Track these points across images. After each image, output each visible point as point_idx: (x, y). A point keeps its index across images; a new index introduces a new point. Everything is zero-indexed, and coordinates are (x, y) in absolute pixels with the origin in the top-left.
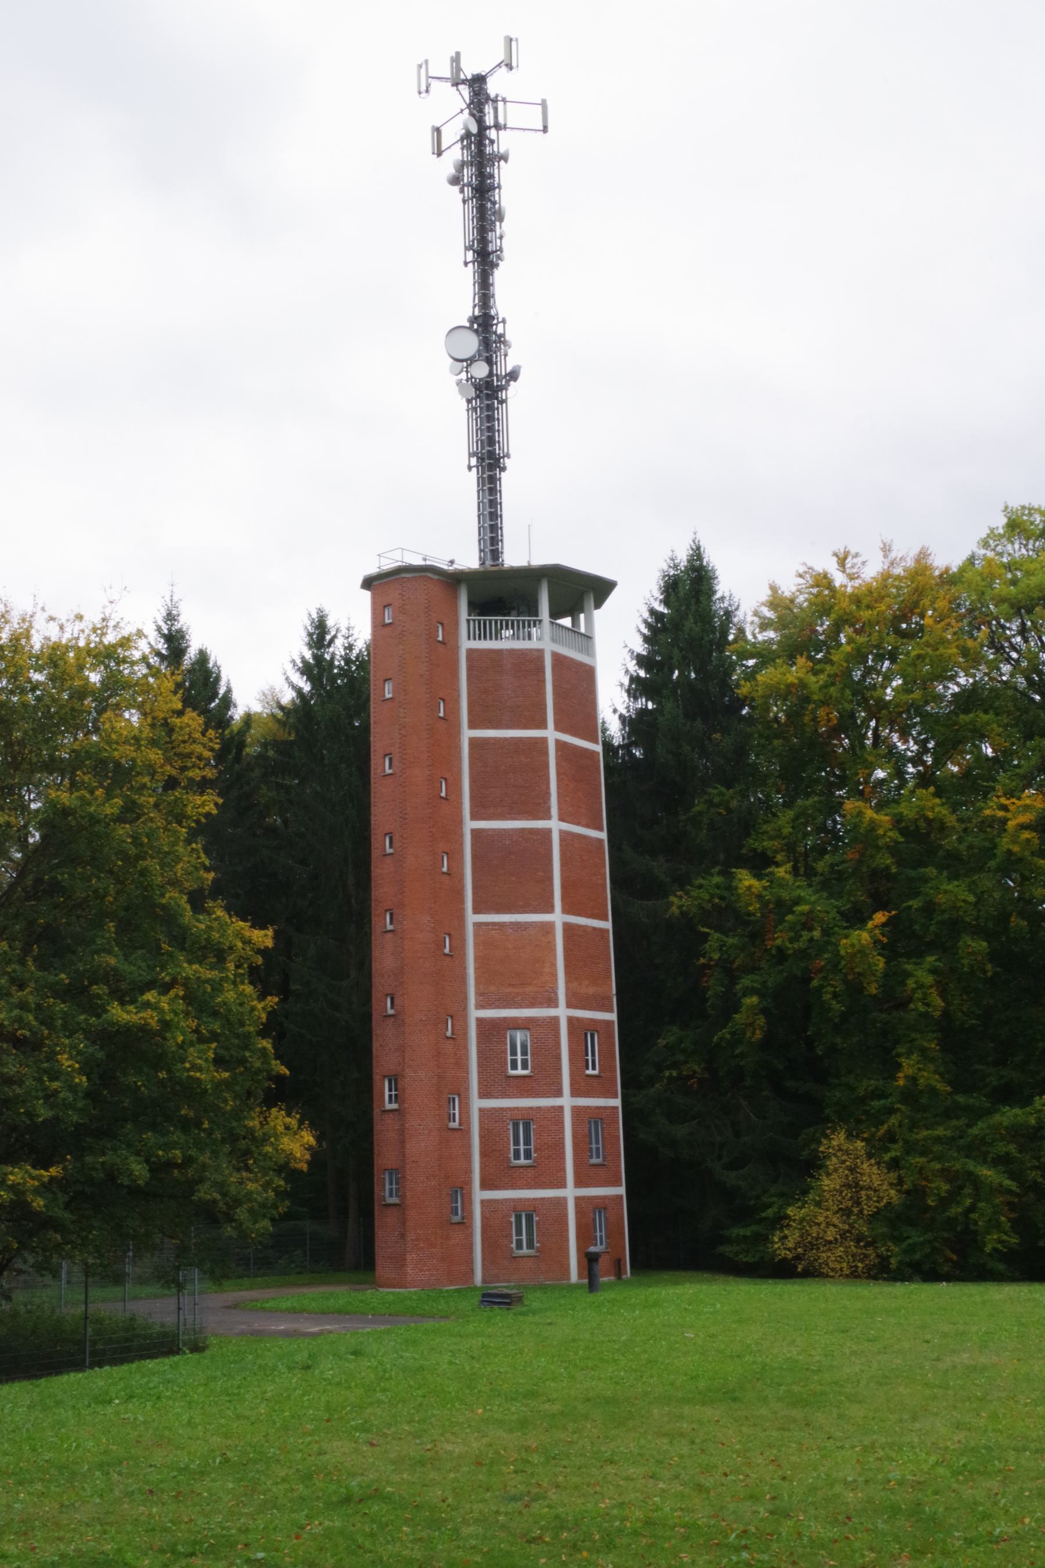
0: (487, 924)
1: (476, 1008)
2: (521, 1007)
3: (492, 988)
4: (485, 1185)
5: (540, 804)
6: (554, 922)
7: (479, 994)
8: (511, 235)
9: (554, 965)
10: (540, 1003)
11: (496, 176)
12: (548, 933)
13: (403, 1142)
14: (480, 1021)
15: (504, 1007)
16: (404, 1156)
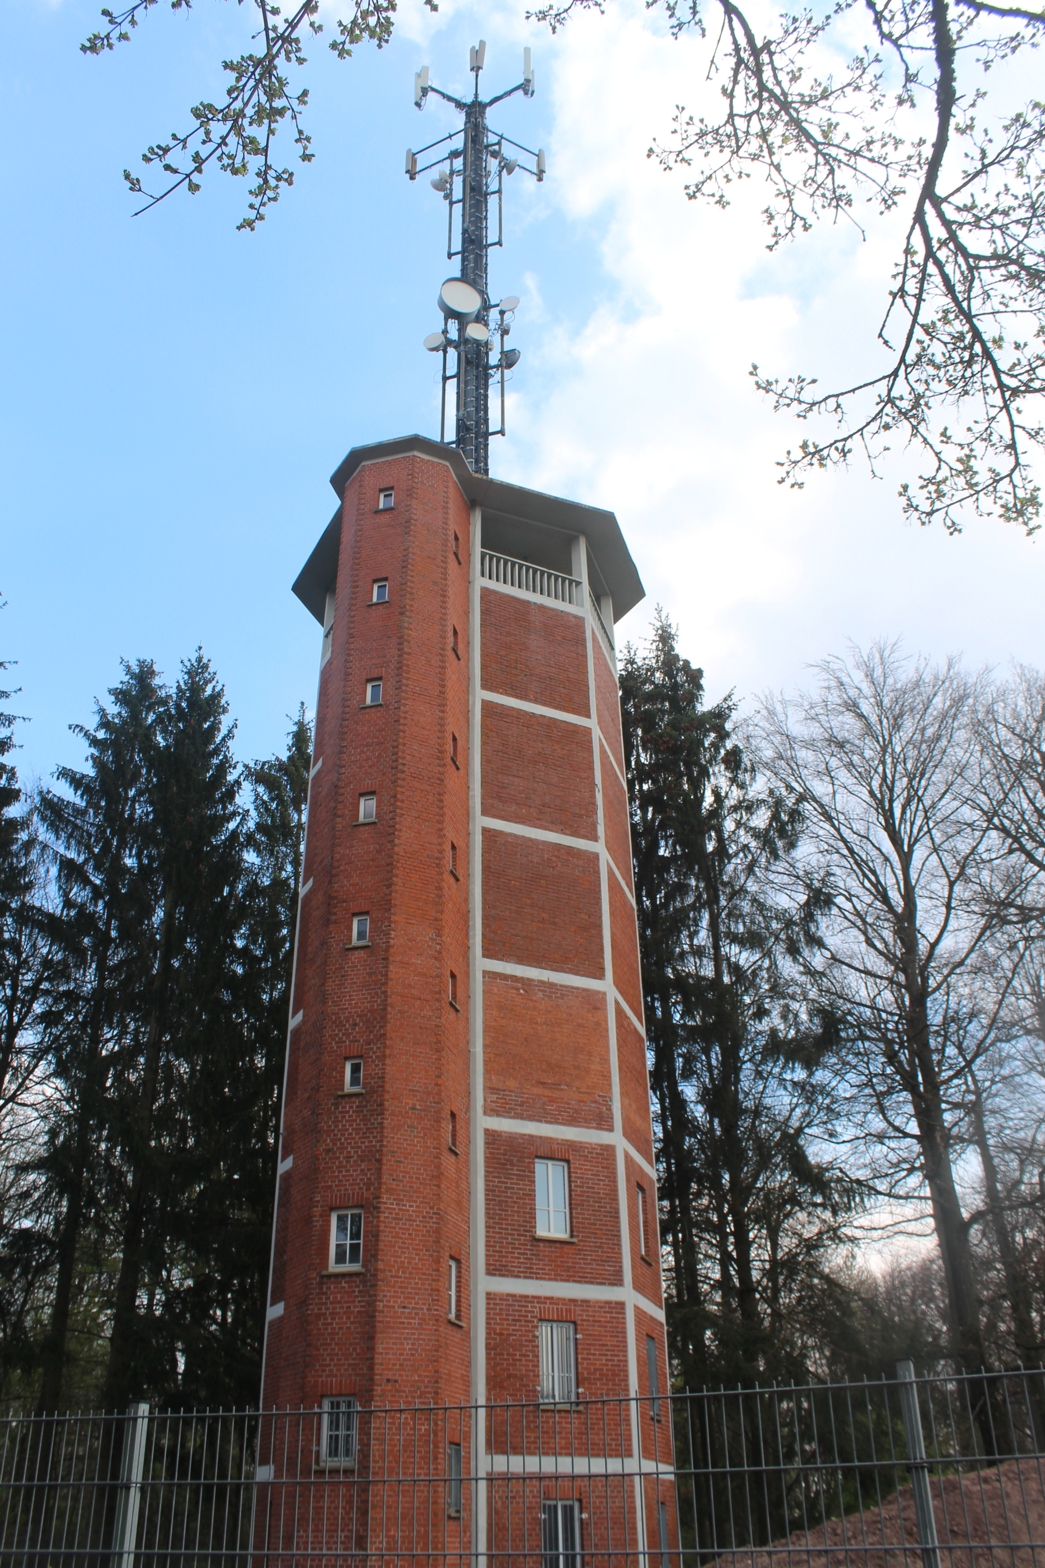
0: (505, 977)
1: (489, 1272)
2: (555, 1121)
3: (512, 1084)
4: (497, 1444)
5: (581, 816)
6: (604, 994)
7: (489, 1089)
8: (445, 101)
9: (605, 1060)
10: (586, 1121)
11: (468, 190)
12: (596, 1008)
13: (369, 1338)
14: (492, 1137)
15: (530, 1118)
16: (371, 1368)
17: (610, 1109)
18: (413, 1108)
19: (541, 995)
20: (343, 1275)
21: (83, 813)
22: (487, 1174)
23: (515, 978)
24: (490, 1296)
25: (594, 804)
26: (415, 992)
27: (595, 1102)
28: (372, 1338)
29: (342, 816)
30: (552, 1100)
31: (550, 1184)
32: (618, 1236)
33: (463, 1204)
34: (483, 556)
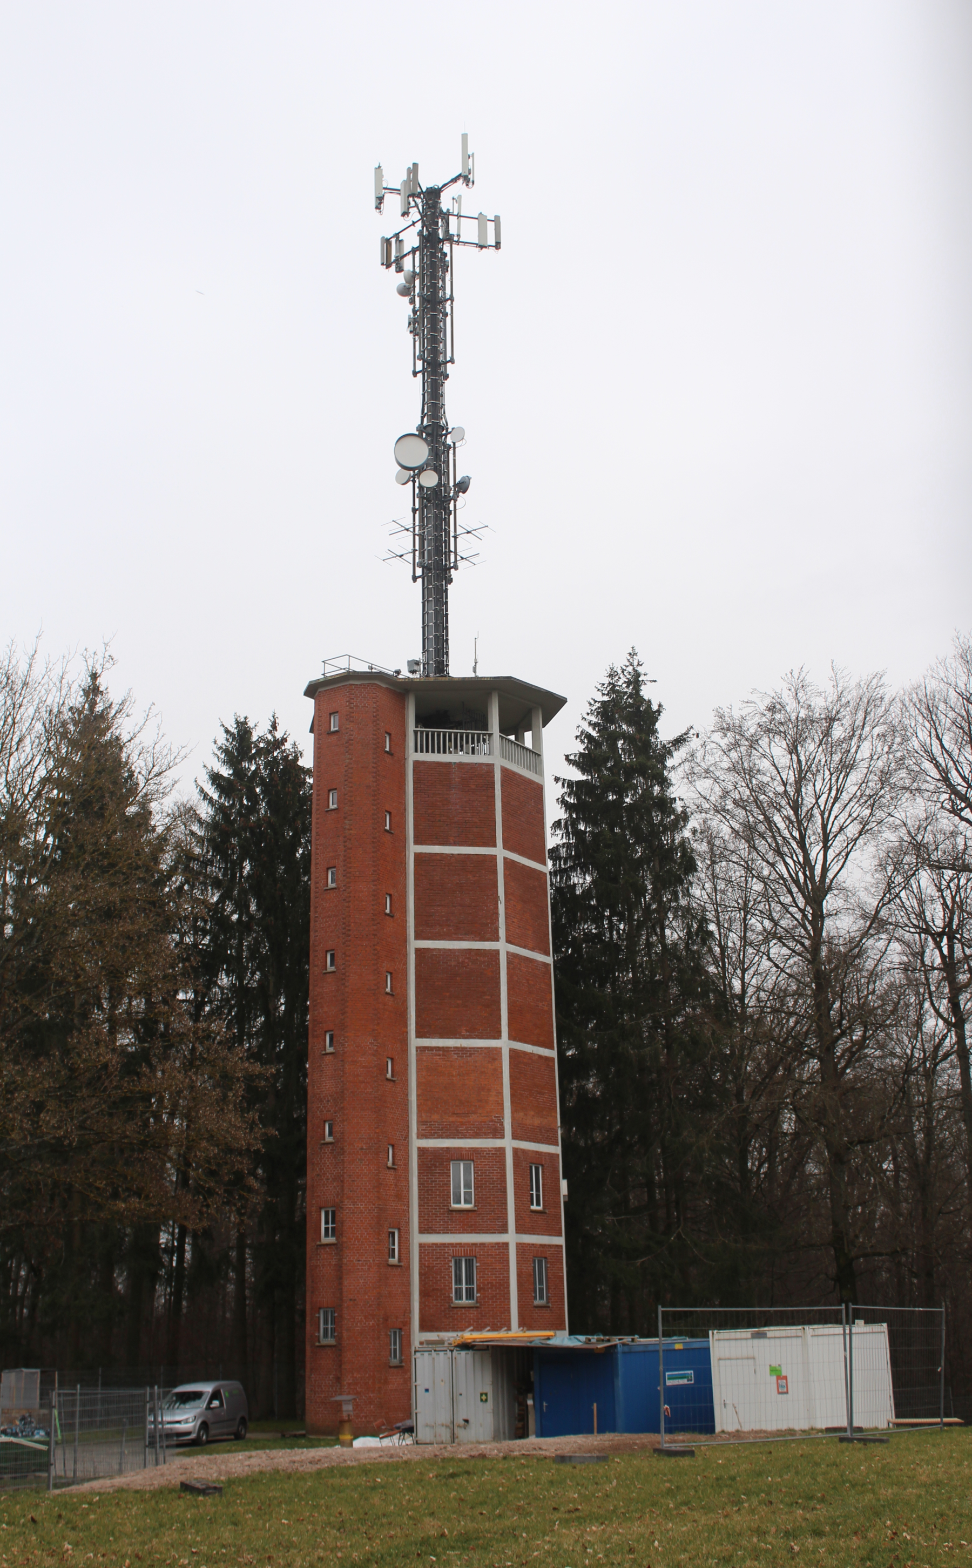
2: (464, 1137)
3: (435, 1117)
5: (487, 924)
7: (420, 1122)
9: (500, 1093)
10: (485, 1134)
12: (494, 1059)
14: (422, 1151)
16: (341, 1293)
17: (502, 1124)
18: (362, 1149)
19: (456, 1056)
20: (327, 1245)
21: (206, 863)
22: (420, 1174)
23: (438, 1048)
24: (421, 1246)
25: (497, 914)
26: (360, 1078)
27: (492, 1121)
28: (341, 1278)
29: (317, 966)
30: (462, 1124)
31: (461, 1177)
32: (506, 1204)
33: (402, 1196)
34: (416, 732)
